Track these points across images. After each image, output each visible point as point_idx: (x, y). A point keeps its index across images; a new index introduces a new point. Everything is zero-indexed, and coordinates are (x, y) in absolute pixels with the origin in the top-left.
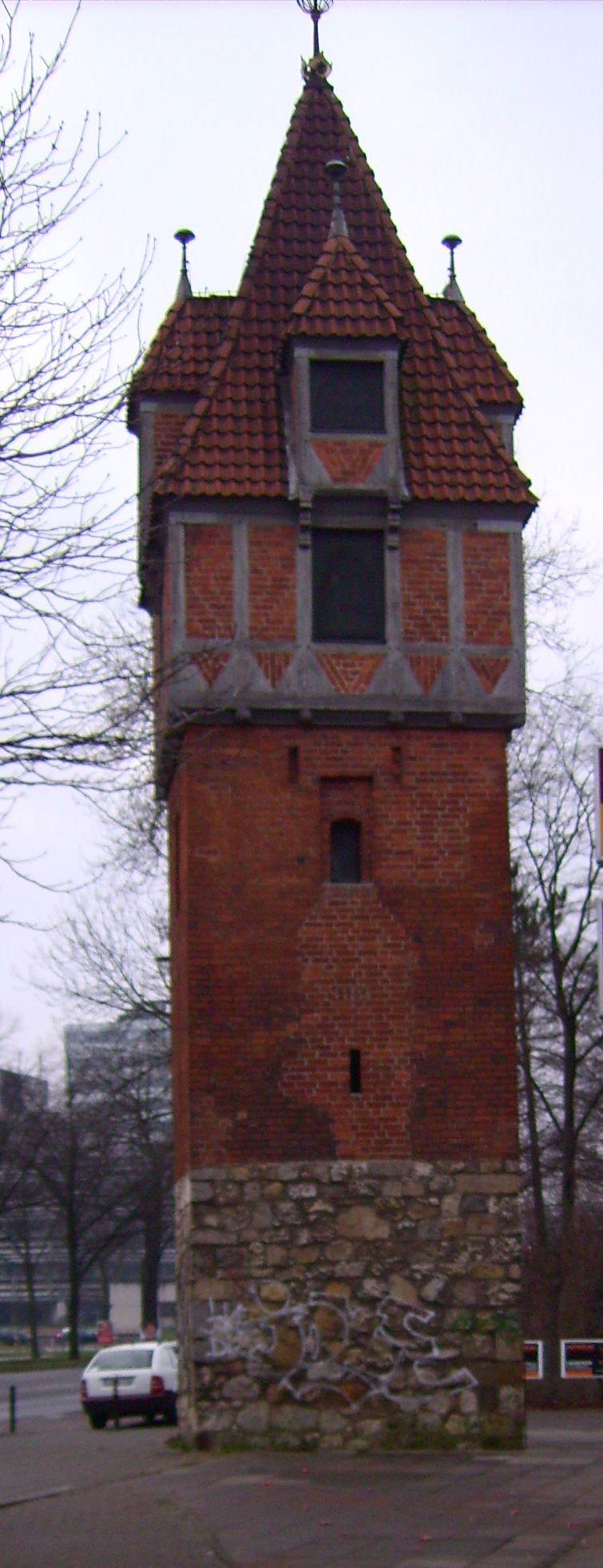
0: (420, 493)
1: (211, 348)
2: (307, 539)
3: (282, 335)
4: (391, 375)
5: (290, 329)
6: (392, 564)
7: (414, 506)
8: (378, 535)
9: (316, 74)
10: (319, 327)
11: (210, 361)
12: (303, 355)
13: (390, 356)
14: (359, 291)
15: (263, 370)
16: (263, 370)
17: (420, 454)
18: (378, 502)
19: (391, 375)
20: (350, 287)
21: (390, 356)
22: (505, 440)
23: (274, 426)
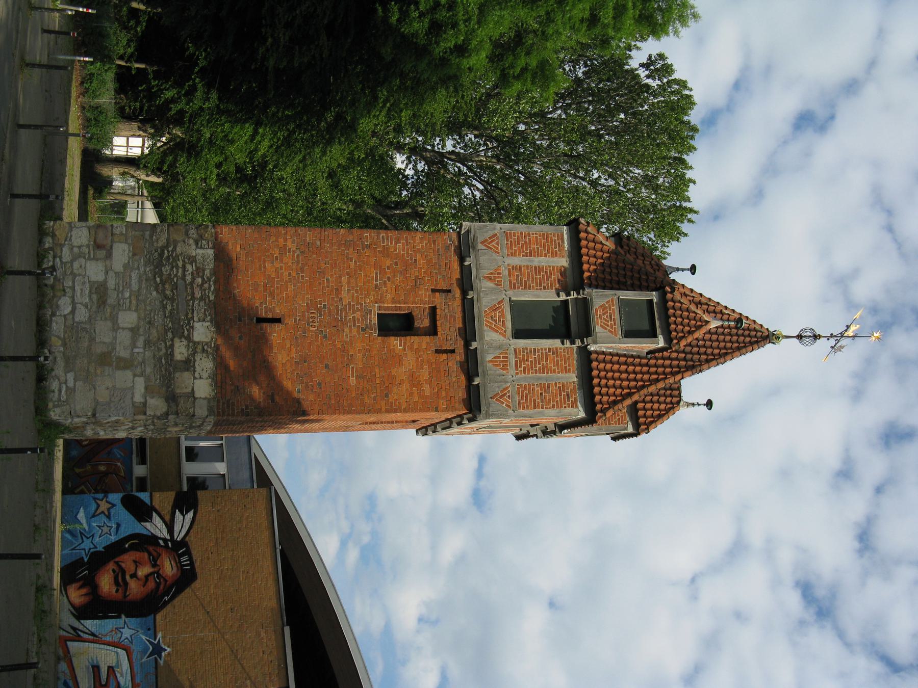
6: (556, 343)
7: (585, 356)
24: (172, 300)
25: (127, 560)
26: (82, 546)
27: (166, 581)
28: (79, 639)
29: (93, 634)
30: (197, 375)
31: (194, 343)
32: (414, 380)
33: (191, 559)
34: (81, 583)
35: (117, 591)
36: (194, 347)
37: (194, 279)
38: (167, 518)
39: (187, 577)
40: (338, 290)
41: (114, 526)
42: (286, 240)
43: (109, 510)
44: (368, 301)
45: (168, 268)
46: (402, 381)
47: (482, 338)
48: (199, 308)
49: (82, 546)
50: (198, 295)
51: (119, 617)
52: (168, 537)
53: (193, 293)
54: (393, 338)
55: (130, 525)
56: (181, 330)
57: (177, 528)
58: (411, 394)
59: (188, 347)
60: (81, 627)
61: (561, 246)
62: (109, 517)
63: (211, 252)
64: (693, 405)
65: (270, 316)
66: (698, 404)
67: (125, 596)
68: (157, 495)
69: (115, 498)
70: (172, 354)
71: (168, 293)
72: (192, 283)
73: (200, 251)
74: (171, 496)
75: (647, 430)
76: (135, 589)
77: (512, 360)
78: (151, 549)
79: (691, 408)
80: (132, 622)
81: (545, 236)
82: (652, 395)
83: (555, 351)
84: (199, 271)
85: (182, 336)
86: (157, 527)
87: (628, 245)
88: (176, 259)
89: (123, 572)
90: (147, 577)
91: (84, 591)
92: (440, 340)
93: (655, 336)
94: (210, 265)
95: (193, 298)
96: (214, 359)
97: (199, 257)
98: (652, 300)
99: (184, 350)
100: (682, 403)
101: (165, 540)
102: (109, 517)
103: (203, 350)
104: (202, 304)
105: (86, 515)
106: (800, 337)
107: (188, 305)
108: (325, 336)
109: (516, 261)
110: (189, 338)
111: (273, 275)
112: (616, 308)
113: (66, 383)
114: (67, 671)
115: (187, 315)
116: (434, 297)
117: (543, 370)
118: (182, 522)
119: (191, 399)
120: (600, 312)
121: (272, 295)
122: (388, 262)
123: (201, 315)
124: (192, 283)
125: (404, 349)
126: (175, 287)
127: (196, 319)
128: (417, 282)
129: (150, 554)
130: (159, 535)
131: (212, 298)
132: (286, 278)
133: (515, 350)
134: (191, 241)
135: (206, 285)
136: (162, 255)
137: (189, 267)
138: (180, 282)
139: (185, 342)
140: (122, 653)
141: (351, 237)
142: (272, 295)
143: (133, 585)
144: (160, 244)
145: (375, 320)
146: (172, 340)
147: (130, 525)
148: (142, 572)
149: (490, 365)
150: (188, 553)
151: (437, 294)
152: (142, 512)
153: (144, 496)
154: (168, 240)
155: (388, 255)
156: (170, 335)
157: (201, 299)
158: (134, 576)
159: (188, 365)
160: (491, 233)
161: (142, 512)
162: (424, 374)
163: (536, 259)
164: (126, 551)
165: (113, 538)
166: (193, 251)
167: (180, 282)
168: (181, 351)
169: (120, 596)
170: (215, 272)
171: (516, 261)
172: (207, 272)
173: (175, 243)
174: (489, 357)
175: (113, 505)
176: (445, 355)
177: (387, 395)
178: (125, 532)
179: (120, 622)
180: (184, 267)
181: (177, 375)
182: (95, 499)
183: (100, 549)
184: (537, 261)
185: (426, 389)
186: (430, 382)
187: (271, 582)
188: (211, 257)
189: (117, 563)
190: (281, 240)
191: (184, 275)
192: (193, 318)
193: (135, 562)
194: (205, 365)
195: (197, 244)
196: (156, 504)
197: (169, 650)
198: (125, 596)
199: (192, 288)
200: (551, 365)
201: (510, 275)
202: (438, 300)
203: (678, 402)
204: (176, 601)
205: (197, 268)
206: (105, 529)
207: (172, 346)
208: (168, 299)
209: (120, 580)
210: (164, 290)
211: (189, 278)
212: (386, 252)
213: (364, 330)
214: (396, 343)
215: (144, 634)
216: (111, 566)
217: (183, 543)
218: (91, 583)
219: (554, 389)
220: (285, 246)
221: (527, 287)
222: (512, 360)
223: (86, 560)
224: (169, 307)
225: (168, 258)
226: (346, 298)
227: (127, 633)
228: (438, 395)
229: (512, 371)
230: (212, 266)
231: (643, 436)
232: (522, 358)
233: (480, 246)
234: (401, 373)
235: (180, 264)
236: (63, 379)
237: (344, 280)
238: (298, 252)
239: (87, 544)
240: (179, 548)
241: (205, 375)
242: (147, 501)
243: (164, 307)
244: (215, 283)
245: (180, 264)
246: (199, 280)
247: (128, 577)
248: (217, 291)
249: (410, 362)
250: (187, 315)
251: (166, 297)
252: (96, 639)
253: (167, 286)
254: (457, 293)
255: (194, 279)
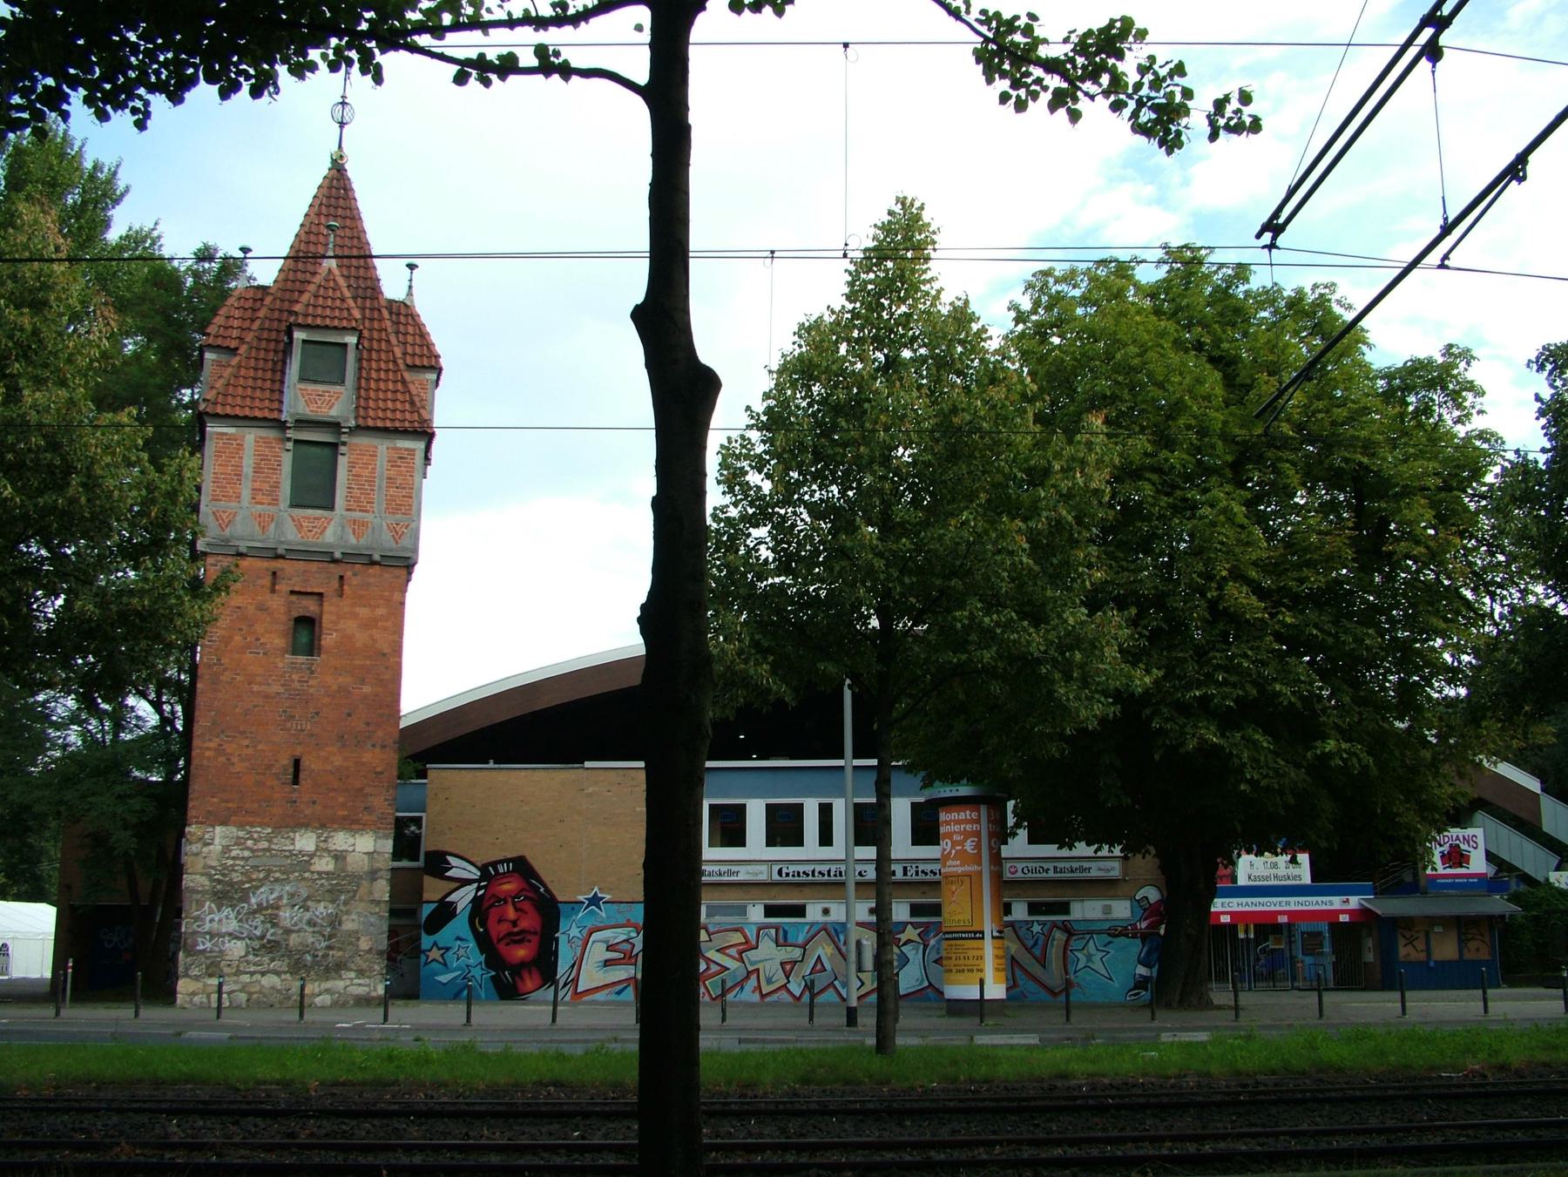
0: (361, 422)
1: (255, 310)
2: (290, 445)
3: (235, 746)
4: (351, 356)
5: (292, 319)
6: (343, 462)
7: (359, 429)
8: (334, 446)
9: (338, 169)
10: (310, 320)
11: (253, 321)
12: (299, 335)
13: (352, 340)
14: (338, 302)
15: (277, 341)
16: (277, 341)
17: (366, 408)
18: (334, 426)
19: (351, 356)
20: (333, 299)
21: (352, 340)
22: (429, 398)
23: (279, 367)
24: (269, 872)
25: (497, 930)
26: (479, 978)
27: (523, 889)
28: (576, 981)
29: (573, 966)
30: (351, 849)
31: (316, 850)
32: (368, 625)
33: (501, 862)
34: (517, 979)
35: (529, 941)
36: (320, 850)
37: (248, 848)
38: (457, 885)
39: (521, 866)
40: (267, 696)
41: (458, 942)
42: (209, 749)
43: (439, 949)
44: (281, 665)
45: (234, 875)
46: (372, 637)
47: (331, 546)
48: (280, 844)
49: (479, 978)
50: (265, 845)
51: (557, 939)
52: (475, 885)
53: (263, 850)
54: (323, 642)
55: (459, 926)
56: (303, 862)
57: (465, 875)
58: (385, 629)
59: (321, 857)
60: (564, 978)
61: (231, 437)
62: (448, 949)
63: (218, 829)
64: (410, 287)
65: (291, 770)
66: (411, 280)
67: (536, 933)
68: (426, 896)
69: (426, 941)
70: (327, 873)
71: (262, 875)
72: (252, 851)
73: (217, 841)
74: (428, 881)
75: (437, 357)
76: (529, 922)
77: (357, 515)
78: (486, 905)
79: (414, 291)
80: (563, 925)
81: (218, 454)
82: (405, 354)
83: (352, 465)
84: (239, 842)
85: (308, 862)
86: (463, 898)
87: (216, 337)
88: (225, 866)
89: (509, 934)
90: (517, 910)
91: (526, 976)
92: (327, 586)
93: (345, 345)
94: (233, 831)
95: (269, 850)
96: (335, 830)
97: (224, 843)
98: (304, 341)
99: (324, 861)
100: (408, 303)
101: (478, 889)
102: (448, 949)
103: (325, 841)
104: (275, 841)
105: (442, 974)
106: (342, 124)
107: (276, 856)
108: (317, 714)
109: (246, 494)
110: (312, 856)
111: (246, 764)
112: (311, 387)
113: (351, 979)
114: (606, 991)
115: (287, 857)
116: (280, 591)
117: (371, 482)
118: (460, 868)
119: (375, 856)
120: (313, 407)
121: (269, 767)
122: (238, 638)
123: (288, 842)
124: (252, 851)
125: (336, 631)
126: (255, 868)
127: (291, 848)
128: (262, 608)
129: (492, 906)
130: (472, 895)
131: (269, 830)
132: (250, 751)
133: (348, 510)
134: (205, 849)
135: (256, 836)
136: (219, 882)
137: (234, 853)
138: (250, 862)
139: (316, 860)
140: (595, 936)
141: (207, 677)
142: (269, 767)
143: (524, 924)
144: (207, 883)
145: (301, 659)
146: (313, 873)
147: (459, 926)
148: (511, 913)
149: (362, 541)
150: (494, 864)
151: (277, 587)
152: (445, 912)
153: (427, 910)
154: (202, 875)
155: (231, 637)
156: (307, 875)
157: (270, 841)
158: (514, 923)
159: (339, 857)
160: (211, 518)
161: (445, 912)
162: (364, 612)
163: (245, 470)
164: (486, 930)
165: (472, 944)
166: (217, 847)
167: (250, 862)
168: (325, 864)
169: (535, 939)
170: (241, 826)
171: (246, 494)
172: (241, 834)
173: (206, 866)
174: (353, 541)
175: (435, 944)
176: (345, 587)
177: (384, 655)
178: (466, 932)
179: (563, 939)
180: (234, 858)
181: (349, 869)
182: (426, 964)
183: (483, 958)
184: (248, 463)
185: (381, 611)
186: (374, 608)
187: (537, 773)
188: (224, 829)
189: (499, 941)
190: (207, 754)
191: (243, 858)
192: (290, 851)
193: (500, 921)
194: (341, 840)
195: (209, 844)
196: (438, 897)
197: (596, 889)
198: (536, 933)
199: (257, 850)
200: (366, 473)
201: (262, 504)
202: (283, 587)
203: (405, 305)
204: (546, 880)
205: (235, 844)
206: (462, 952)
207: (319, 873)
208: (268, 875)
209: (517, 938)
210: (260, 880)
211: (247, 854)
212: (227, 640)
213: (312, 673)
214: (328, 639)
215: (577, 914)
216: (502, 947)
217: (484, 869)
218: (518, 969)
219: (392, 473)
220: (215, 750)
221: (276, 486)
222: (357, 515)
223: (493, 973)
224: (277, 875)
225: (224, 875)
226: (276, 688)
227: (574, 932)
228: (388, 600)
229: (369, 517)
230: (234, 829)
231: (443, 362)
232: (355, 504)
233: (227, 532)
234: (361, 638)
235: (230, 862)
236: (348, 982)
237: (256, 688)
238: (222, 736)
239: (477, 972)
240: (488, 873)
241: (351, 840)
242: (434, 906)
243: (277, 880)
244: (252, 826)
245: (230, 862)
246: (250, 843)
247: (516, 930)
248: (261, 825)
249: (350, 626)
250: (287, 857)
251: (266, 878)
252: (577, 964)
253: (254, 876)
254: (279, 564)
255: (248, 848)
